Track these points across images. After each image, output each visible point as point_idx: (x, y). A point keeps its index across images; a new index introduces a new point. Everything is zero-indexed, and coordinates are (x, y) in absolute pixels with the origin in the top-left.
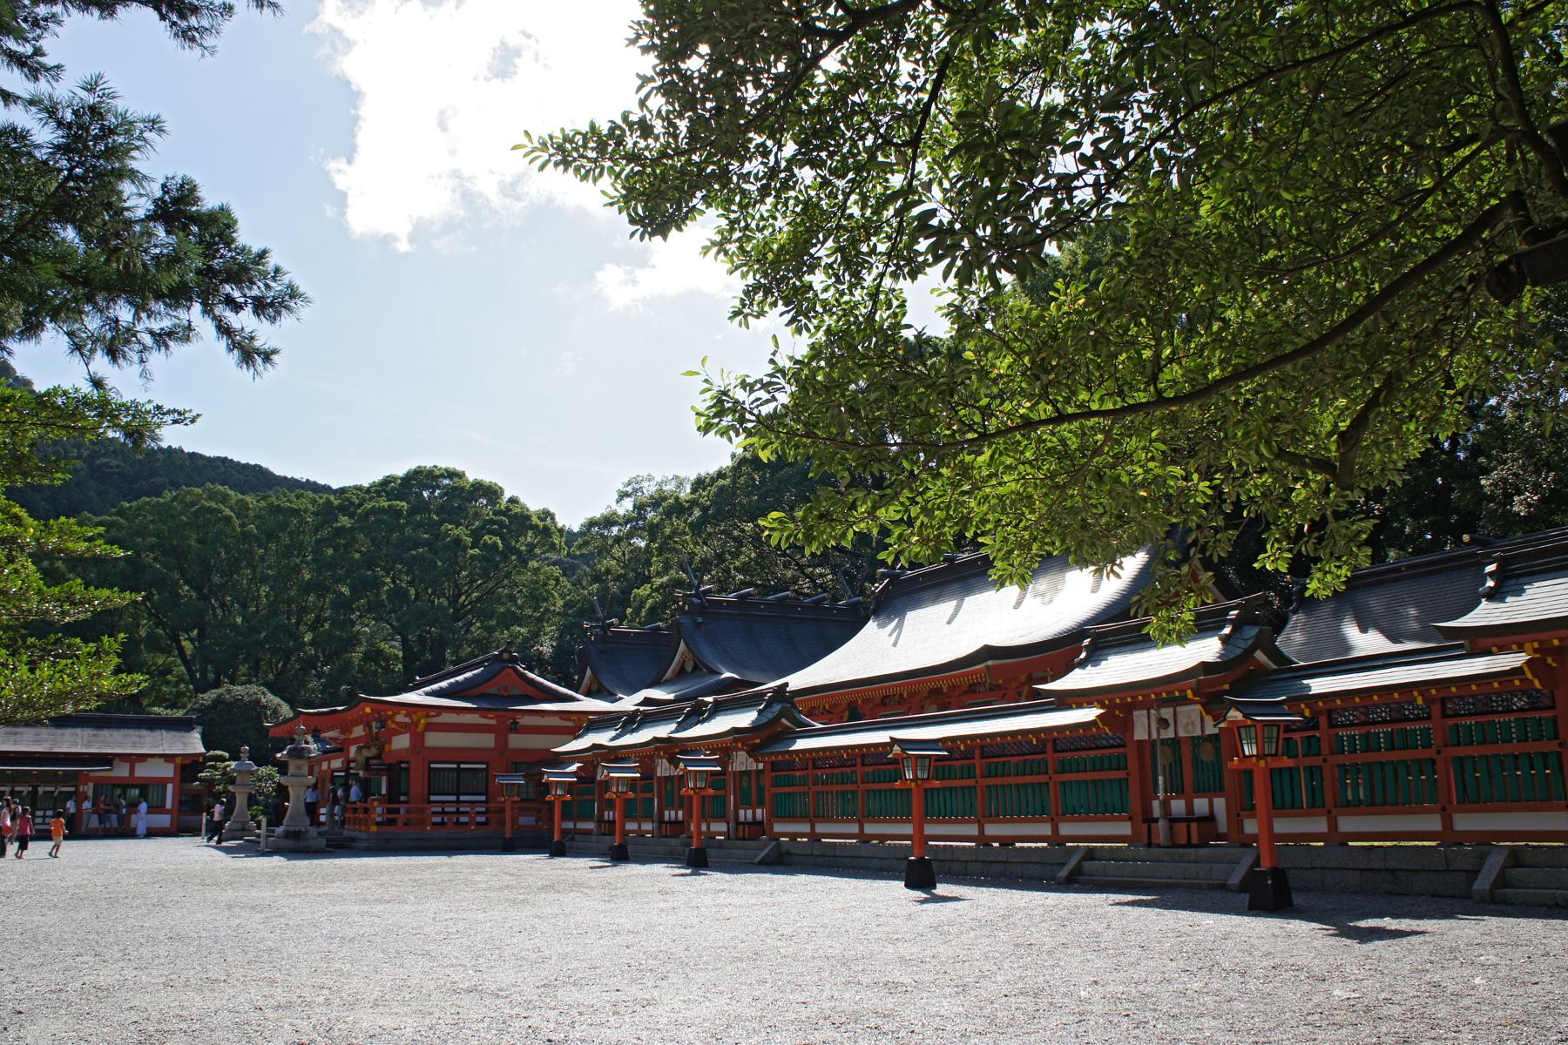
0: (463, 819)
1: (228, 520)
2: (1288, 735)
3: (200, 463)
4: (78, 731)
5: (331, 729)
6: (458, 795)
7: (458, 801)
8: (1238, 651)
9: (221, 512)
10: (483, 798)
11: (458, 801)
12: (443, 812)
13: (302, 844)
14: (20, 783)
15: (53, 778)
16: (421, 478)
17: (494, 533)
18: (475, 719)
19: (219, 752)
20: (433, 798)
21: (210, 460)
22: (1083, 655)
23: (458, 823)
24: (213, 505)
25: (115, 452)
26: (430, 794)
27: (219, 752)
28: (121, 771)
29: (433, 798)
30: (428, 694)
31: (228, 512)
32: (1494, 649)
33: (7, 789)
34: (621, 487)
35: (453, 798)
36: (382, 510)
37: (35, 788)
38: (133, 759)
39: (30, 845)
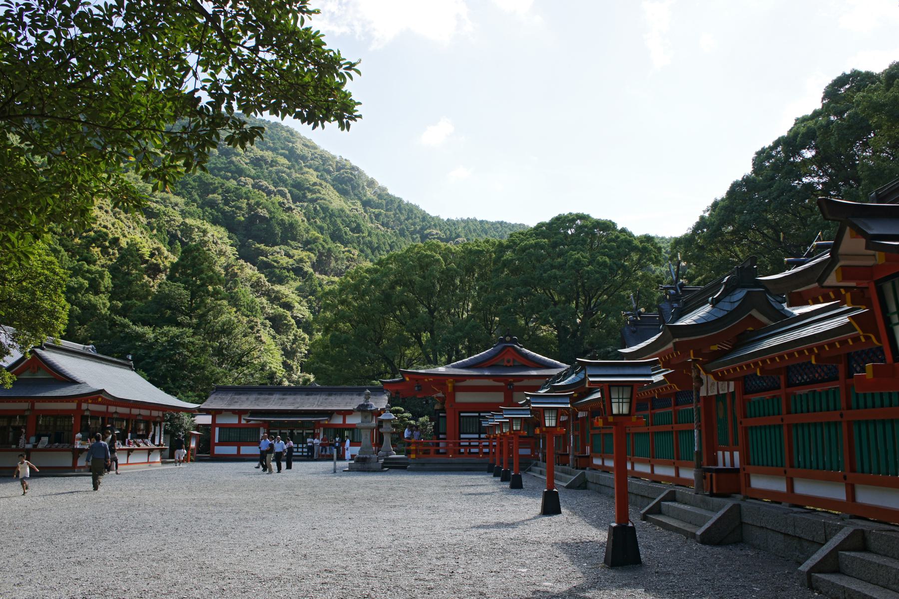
0: (473, 450)
1: (438, 260)
2: (789, 390)
3: (486, 226)
4: (318, 397)
5: (660, 382)
6: (479, 434)
7: (480, 438)
8: (720, 314)
9: (433, 257)
11: (480, 438)
13: (366, 466)
14: (285, 428)
15: (302, 425)
16: (561, 222)
17: (604, 254)
18: (490, 383)
19: (397, 408)
21: (493, 224)
23: (470, 453)
24: (429, 253)
25: (435, 225)
26: (460, 433)
27: (397, 408)
28: (338, 420)
29: (462, 436)
30: (454, 367)
31: (438, 256)
32: (810, 301)
33: (277, 431)
34: (702, 214)
35: (477, 436)
36: (532, 246)
37: (292, 431)
38: (330, 414)
39: (294, 464)
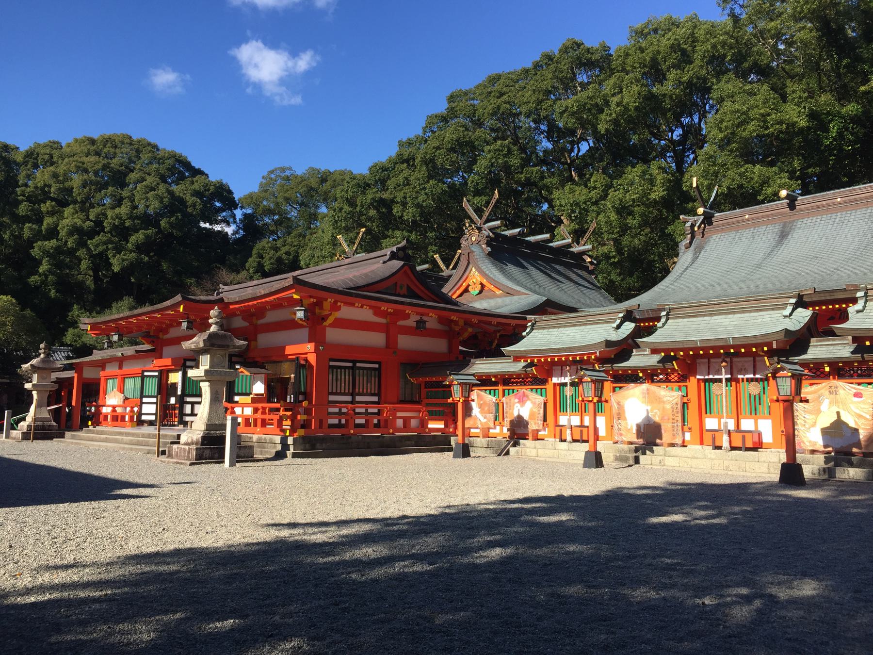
10: (375, 399)
12: (367, 413)
20: (332, 398)
22: (528, 330)
29: (332, 398)
35: (348, 398)
